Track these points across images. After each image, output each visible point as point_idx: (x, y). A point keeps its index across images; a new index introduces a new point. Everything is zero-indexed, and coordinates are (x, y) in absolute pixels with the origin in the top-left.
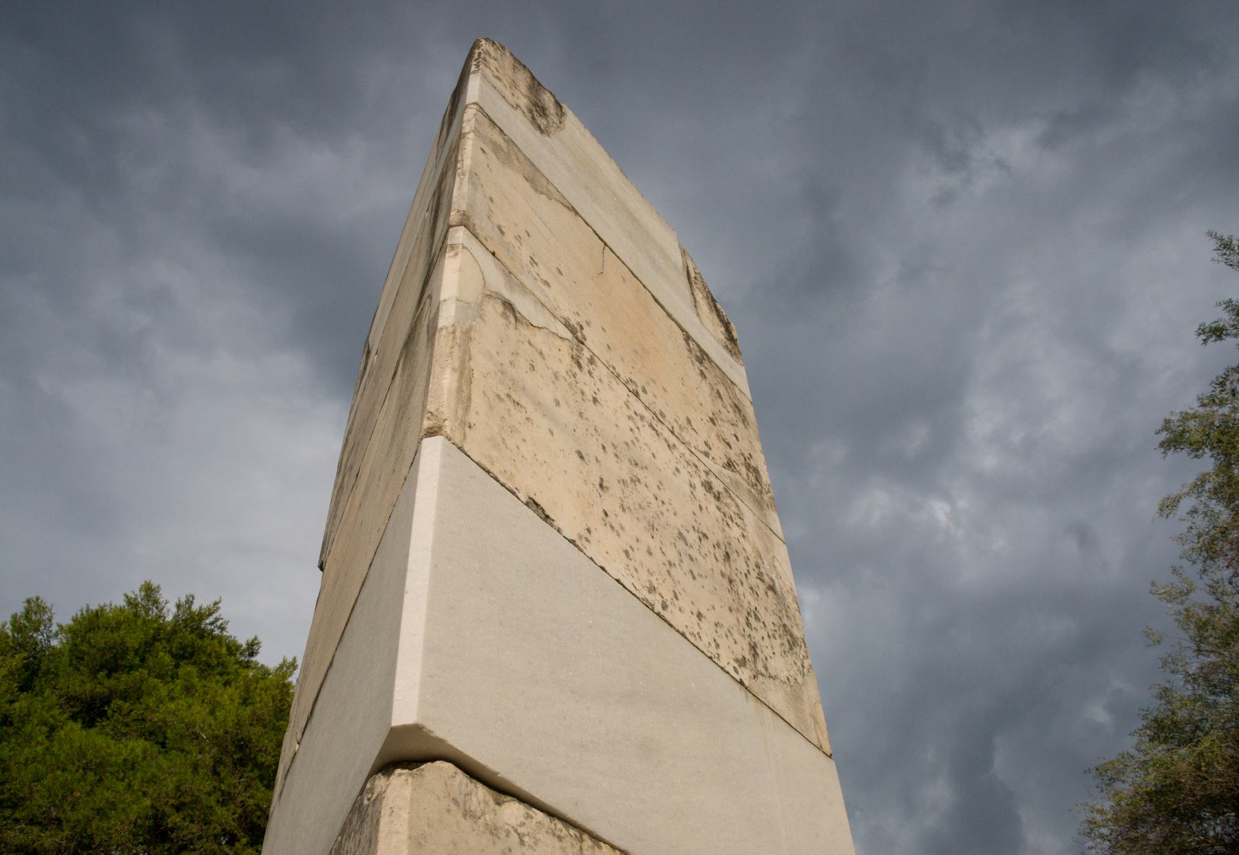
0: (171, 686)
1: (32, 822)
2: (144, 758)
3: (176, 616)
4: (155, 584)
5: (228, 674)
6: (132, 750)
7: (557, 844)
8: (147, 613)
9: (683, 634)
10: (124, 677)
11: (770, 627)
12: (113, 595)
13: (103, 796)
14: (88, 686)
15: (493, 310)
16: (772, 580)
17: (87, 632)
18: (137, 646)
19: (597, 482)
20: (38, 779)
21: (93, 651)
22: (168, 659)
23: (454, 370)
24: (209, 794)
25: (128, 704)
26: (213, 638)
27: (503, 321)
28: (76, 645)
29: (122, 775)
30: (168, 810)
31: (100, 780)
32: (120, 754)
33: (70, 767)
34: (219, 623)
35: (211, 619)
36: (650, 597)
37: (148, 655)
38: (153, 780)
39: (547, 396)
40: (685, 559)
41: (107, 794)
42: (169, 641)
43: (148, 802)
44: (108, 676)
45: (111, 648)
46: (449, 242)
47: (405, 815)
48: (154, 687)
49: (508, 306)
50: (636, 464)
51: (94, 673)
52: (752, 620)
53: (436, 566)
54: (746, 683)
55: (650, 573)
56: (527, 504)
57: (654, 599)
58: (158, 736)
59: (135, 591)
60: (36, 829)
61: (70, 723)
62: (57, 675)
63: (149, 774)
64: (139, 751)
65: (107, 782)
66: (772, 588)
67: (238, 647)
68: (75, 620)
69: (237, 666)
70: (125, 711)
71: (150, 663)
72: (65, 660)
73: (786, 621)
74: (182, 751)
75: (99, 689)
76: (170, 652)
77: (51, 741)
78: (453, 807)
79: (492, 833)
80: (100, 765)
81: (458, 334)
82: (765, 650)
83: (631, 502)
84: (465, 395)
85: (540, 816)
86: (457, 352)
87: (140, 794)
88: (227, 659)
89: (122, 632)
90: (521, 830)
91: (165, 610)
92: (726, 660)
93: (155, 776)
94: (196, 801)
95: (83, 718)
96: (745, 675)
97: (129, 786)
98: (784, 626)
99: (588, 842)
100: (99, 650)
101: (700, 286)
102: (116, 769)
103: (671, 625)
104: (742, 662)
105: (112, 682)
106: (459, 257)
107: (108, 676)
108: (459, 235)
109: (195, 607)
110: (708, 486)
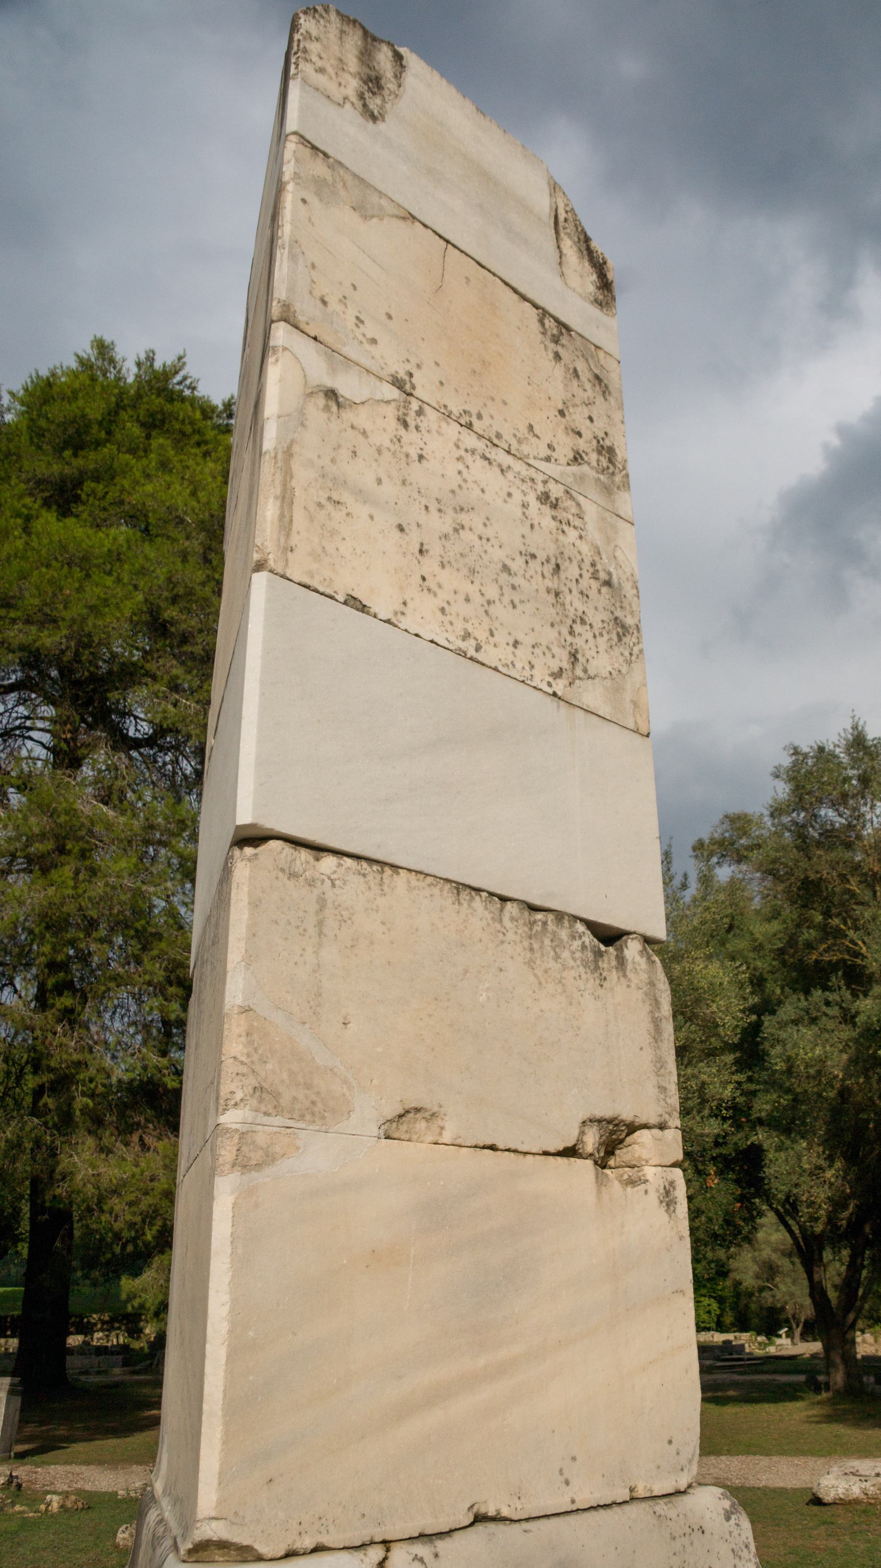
0: (145, 461)
1: (28, 621)
2: (129, 548)
3: (138, 376)
4: (108, 339)
5: (206, 442)
6: (115, 539)
7: (362, 879)
8: (104, 375)
9: (496, 669)
10: (92, 455)
11: (598, 625)
12: (61, 351)
13: (93, 593)
14: (56, 468)
15: (316, 406)
16: (610, 574)
17: (41, 407)
18: (100, 418)
19: (418, 547)
20: (24, 576)
21: (53, 427)
22: (136, 431)
23: (276, 498)
24: (203, 584)
25: (101, 487)
26: (183, 400)
27: (325, 415)
28: (32, 420)
29: (109, 566)
30: (163, 605)
31: (88, 576)
32: (103, 546)
33: (54, 563)
34: (188, 382)
35: (178, 378)
36: (463, 645)
37: (113, 427)
38: (142, 572)
39: (368, 479)
40: (507, 590)
41: (97, 590)
42: (134, 407)
43: (140, 597)
44: (75, 455)
45: (73, 421)
46: (272, 343)
47: (246, 889)
48: (127, 464)
49: (331, 394)
50: (462, 509)
51: (59, 450)
52: (578, 628)
53: (263, 694)
54: (559, 693)
55: (466, 620)
56: (345, 603)
57: (469, 647)
58: (137, 518)
59: (87, 350)
60: (34, 629)
61: (44, 512)
62: (19, 457)
63: (137, 566)
64: (121, 539)
65: (95, 577)
66: (608, 583)
67: (214, 409)
68: (26, 390)
69: (215, 432)
70: (100, 494)
71: (118, 436)
72: (25, 438)
73: (619, 613)
74: (168, 538)
75: (67, 471)
76: (138, 420)
77: (29, 534)
78: (280, 874)
79: (310, 885)
80: (85, 558)
81: (280, 456)
82: (587, 651)
83: (451, 554)
84: (287, 520)
85: (348, 862)
86: (279, 478)
87: (131, 588)
88: (201, 424)
89: (80, 403)
90: (333, 877)
91: (124, 370)
92: (540, 677)
93: (143, 568)
94: (190, 593)
95: (56, 502)
96: (559, 686)
97: (119, 580)
98: (616, 619)
99: (388, 871)
100: (59, 425)
101: (571, 228)
102: (100, 561)
103: (483, 664)
104: (558, 674)
105: (79, 462)
106: (279, 364)
107: (75, 455)
108: (281, 334)
109: (158, 365)
110: (544, 498)
